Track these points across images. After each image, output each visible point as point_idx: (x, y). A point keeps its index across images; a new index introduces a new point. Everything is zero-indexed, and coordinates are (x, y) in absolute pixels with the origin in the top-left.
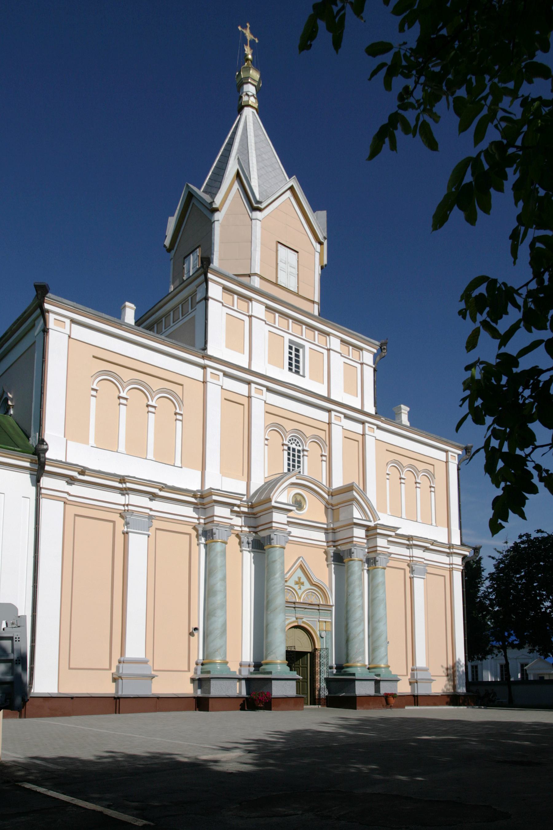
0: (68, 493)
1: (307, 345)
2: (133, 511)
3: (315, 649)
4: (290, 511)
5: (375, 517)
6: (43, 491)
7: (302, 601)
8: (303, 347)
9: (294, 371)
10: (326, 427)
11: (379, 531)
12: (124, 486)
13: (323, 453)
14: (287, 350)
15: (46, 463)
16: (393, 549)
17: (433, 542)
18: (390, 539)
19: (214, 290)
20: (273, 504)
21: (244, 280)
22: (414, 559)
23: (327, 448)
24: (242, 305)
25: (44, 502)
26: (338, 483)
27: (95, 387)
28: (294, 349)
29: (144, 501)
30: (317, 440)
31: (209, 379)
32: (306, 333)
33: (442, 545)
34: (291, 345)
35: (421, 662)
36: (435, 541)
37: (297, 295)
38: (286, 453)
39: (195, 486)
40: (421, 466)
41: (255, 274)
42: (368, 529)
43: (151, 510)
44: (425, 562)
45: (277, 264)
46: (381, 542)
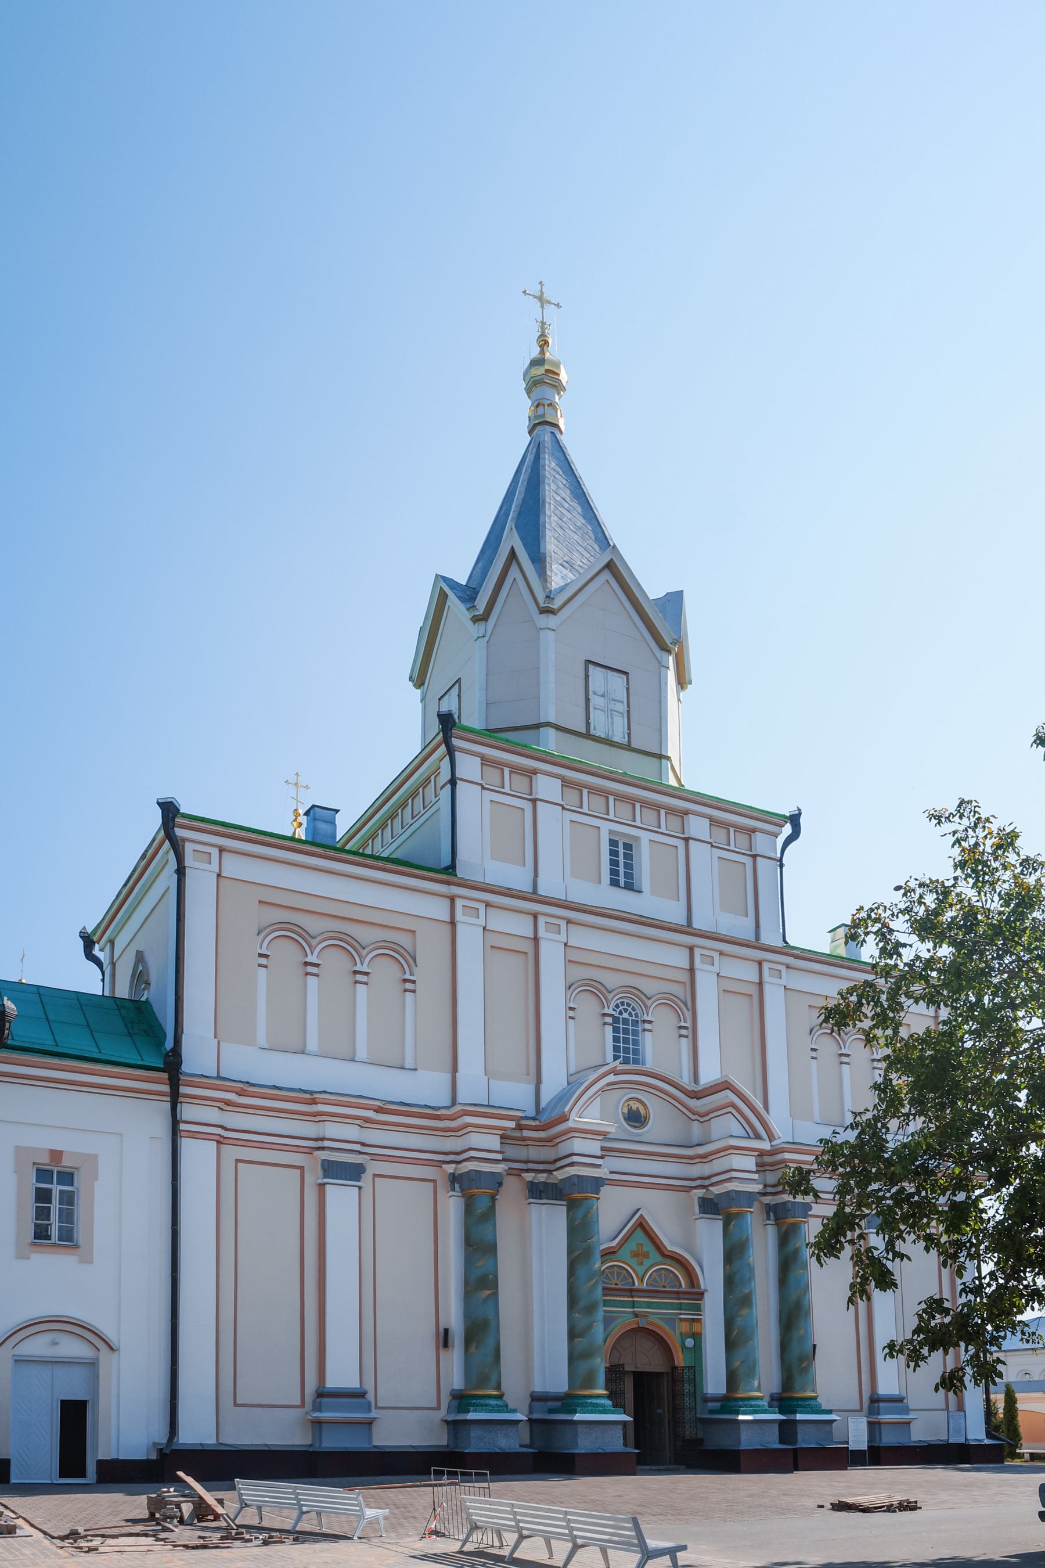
3: (674, 1368)
8: (637, 839)
9: (622, 884)
14: (605, 848)
24: (520, 783)
25: (187, 1145)
28: (621, 845)
30: (669, 1001)
31: (542, 933)
38: (609, 1030)
39: (441, 1098)
41: (548, 724)
43: (363, 1144)
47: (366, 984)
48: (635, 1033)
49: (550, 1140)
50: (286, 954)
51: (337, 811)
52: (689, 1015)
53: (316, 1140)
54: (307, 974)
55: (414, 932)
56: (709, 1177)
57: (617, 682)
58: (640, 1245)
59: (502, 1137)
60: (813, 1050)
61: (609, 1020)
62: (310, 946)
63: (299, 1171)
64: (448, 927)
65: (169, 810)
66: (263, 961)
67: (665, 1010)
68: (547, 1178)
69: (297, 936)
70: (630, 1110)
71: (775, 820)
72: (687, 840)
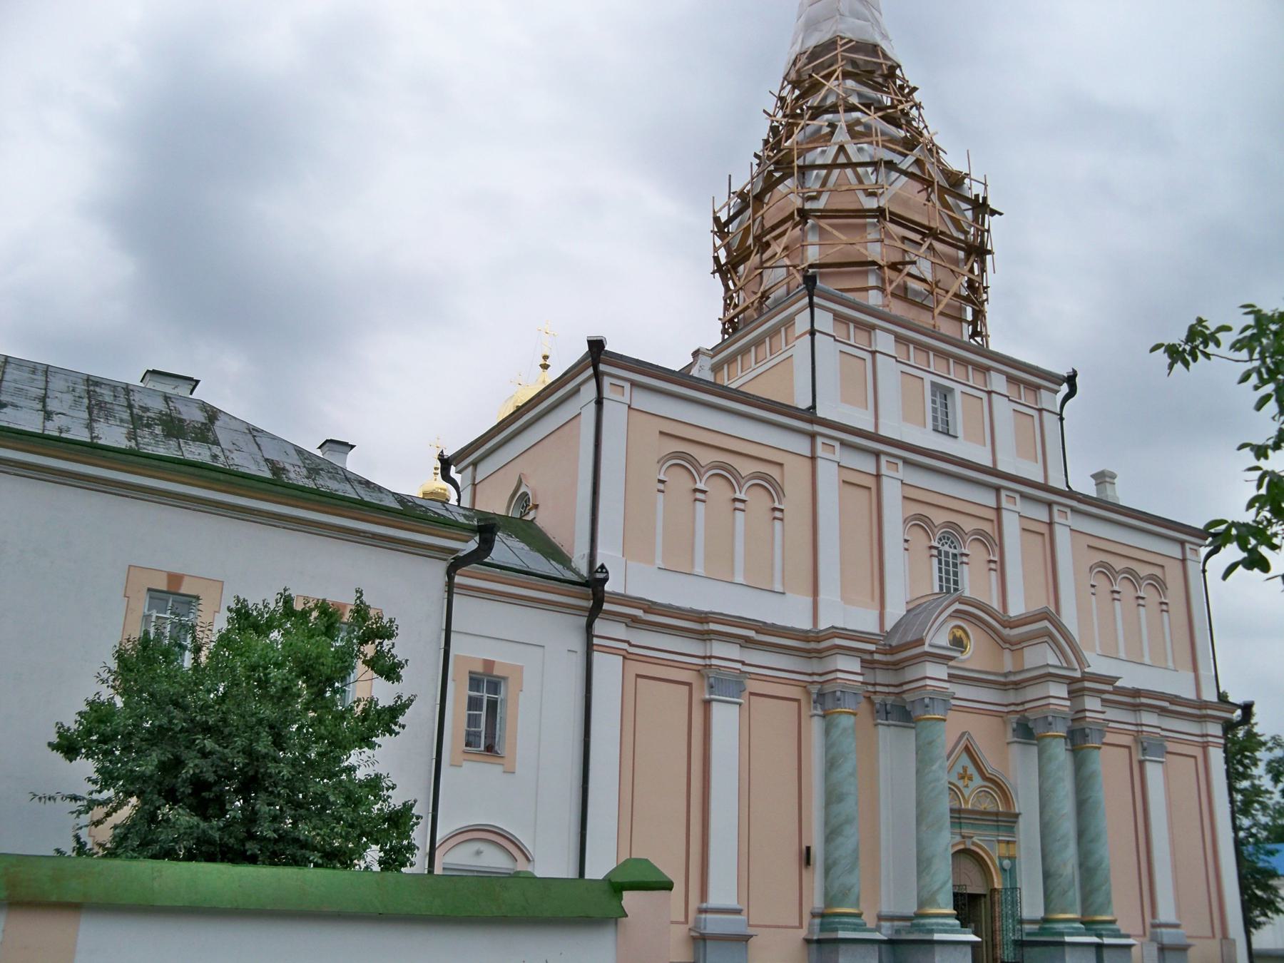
1: (958, 388)
8: (951, 390)
10: (992, 515)
16: (1112, 714)
17: (1174, 699)
22: (714, 662)
27: (662, 477)
29: (733, 651)
30: (981, 538)
32: (955, 371)
35: (1166, 912)
38: (935, 561)
43: (743, 663)
46: (1092, 703)
47: (704, 501)
48: (955, 565)
49: (895, 664)
50: (680, 482)
52: (997, 550)
53: (704, 658)
54: (696, 500)
55: (781, 465)
58: (965, 769)
59: (863, 661)
60: (660, 481)
61: (935, 552)
62: (738, 483)
63: (796, 704)
64: (808, 463)
67: (978, 546)
68: (1216, 745)
69: (683, 461)
70: (955, 637)
71: (1056, 379)
72: (873, 353)
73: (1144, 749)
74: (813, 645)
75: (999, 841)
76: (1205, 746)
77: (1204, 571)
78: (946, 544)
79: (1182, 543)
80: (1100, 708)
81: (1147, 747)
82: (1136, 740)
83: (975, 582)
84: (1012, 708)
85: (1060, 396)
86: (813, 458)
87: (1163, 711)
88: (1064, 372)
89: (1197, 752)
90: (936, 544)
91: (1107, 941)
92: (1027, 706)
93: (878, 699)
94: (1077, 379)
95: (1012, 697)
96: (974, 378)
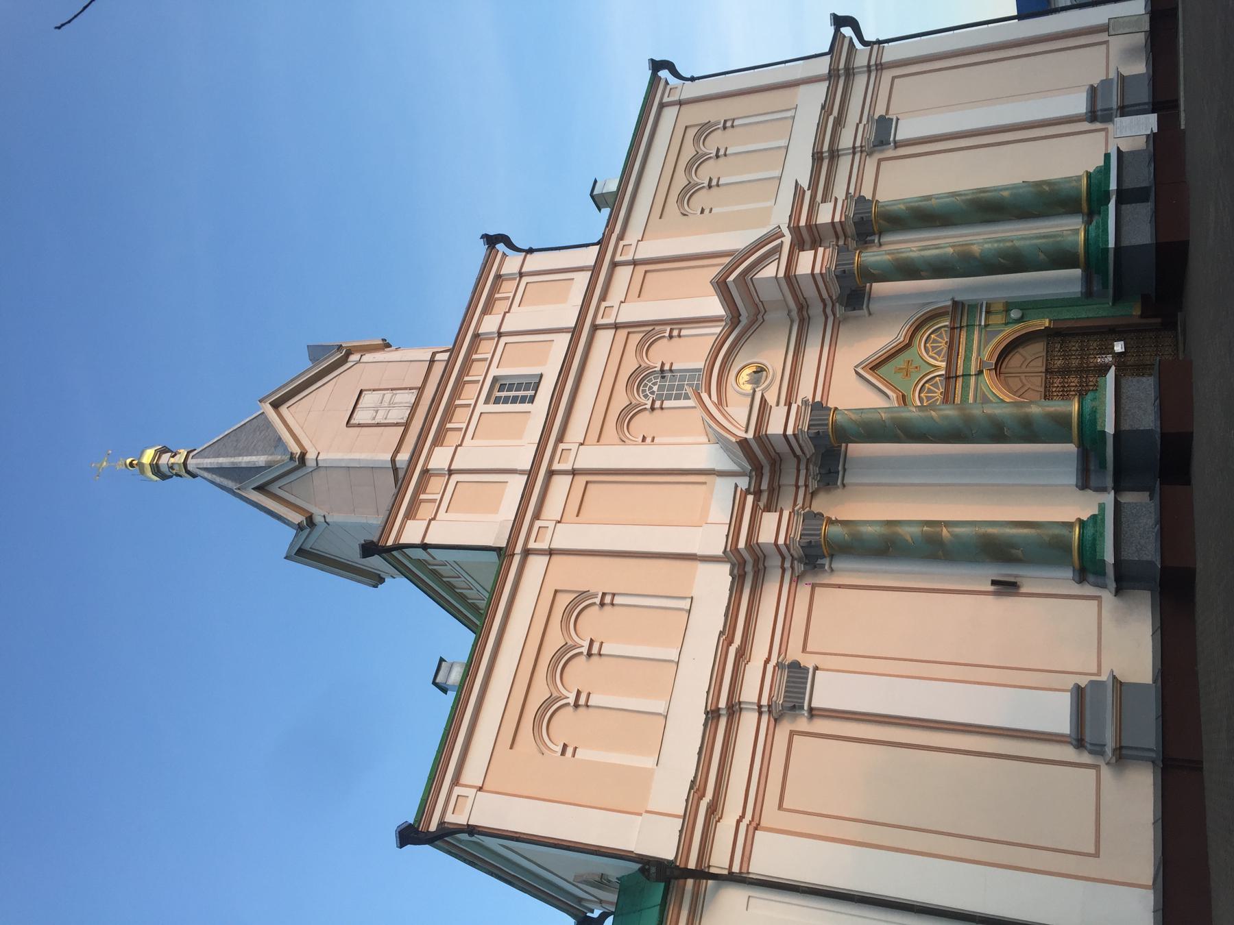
0: (739, 822)
1: (494, 372)
2: (770, 698)
4: (763, 401)
5: (778, 234)
6: (736, 869)
7: (944, 364)
8: (495, 379)
10: (622, 333)
11: (803, 223)
12: (723, 712)
13: (667, 334)
15: (682, 866)
16: (839, 191)
17: (826, 108)
18: (819, 198)
19: (412, 533)
20: (750, 435)
21: (401, 474)
23: (657, 328)
25: (760, 867)
26: (715, 307)
27: (559, 749)
30: (645, 346)
32: (477, 371)
33: (831, 95)
34: (493, 400)
36: (823, 107)
37: (421, 390)
38: (667, 404)
39: (721, 575)
40: (689, 152)
41: (393, 461)
42: (799, 244)
43: (767, 661)
44: (864, 121)
45: (378, 425)
46: (825, 215)
50: (565, 724)
51: (442, 660)
55: (556, 591)
56: (823, 300)
57: (367, 399)
61: (658, 404)
64: (555, 558)
65: (409, 835)
66: (570, 751)
73: (794, 708)
74: (749, 568)
75: (986, 326)
76: (881, 67)
77: (693, 79)
78: (654, 386)
79: (662, 106)
80: (832, 204)
81: (882, 135)
82: (870, 154)
83: (689, 354)
84: (829, 311)
85: (673, 81)
86: (551, 552)
87: (839, 122)
88: (482, 248)
89: (887, 76)
90: (649, 403)
91: (1113, 186)
92: (825, 295)
93: (813, 485)
94: (491, 233)
95: (816, 310)
96: (485, 349)
